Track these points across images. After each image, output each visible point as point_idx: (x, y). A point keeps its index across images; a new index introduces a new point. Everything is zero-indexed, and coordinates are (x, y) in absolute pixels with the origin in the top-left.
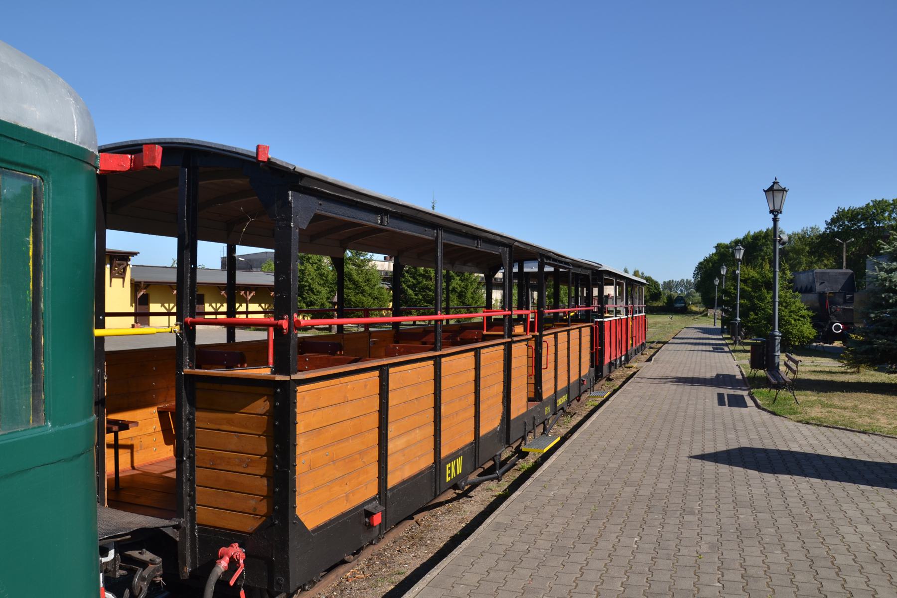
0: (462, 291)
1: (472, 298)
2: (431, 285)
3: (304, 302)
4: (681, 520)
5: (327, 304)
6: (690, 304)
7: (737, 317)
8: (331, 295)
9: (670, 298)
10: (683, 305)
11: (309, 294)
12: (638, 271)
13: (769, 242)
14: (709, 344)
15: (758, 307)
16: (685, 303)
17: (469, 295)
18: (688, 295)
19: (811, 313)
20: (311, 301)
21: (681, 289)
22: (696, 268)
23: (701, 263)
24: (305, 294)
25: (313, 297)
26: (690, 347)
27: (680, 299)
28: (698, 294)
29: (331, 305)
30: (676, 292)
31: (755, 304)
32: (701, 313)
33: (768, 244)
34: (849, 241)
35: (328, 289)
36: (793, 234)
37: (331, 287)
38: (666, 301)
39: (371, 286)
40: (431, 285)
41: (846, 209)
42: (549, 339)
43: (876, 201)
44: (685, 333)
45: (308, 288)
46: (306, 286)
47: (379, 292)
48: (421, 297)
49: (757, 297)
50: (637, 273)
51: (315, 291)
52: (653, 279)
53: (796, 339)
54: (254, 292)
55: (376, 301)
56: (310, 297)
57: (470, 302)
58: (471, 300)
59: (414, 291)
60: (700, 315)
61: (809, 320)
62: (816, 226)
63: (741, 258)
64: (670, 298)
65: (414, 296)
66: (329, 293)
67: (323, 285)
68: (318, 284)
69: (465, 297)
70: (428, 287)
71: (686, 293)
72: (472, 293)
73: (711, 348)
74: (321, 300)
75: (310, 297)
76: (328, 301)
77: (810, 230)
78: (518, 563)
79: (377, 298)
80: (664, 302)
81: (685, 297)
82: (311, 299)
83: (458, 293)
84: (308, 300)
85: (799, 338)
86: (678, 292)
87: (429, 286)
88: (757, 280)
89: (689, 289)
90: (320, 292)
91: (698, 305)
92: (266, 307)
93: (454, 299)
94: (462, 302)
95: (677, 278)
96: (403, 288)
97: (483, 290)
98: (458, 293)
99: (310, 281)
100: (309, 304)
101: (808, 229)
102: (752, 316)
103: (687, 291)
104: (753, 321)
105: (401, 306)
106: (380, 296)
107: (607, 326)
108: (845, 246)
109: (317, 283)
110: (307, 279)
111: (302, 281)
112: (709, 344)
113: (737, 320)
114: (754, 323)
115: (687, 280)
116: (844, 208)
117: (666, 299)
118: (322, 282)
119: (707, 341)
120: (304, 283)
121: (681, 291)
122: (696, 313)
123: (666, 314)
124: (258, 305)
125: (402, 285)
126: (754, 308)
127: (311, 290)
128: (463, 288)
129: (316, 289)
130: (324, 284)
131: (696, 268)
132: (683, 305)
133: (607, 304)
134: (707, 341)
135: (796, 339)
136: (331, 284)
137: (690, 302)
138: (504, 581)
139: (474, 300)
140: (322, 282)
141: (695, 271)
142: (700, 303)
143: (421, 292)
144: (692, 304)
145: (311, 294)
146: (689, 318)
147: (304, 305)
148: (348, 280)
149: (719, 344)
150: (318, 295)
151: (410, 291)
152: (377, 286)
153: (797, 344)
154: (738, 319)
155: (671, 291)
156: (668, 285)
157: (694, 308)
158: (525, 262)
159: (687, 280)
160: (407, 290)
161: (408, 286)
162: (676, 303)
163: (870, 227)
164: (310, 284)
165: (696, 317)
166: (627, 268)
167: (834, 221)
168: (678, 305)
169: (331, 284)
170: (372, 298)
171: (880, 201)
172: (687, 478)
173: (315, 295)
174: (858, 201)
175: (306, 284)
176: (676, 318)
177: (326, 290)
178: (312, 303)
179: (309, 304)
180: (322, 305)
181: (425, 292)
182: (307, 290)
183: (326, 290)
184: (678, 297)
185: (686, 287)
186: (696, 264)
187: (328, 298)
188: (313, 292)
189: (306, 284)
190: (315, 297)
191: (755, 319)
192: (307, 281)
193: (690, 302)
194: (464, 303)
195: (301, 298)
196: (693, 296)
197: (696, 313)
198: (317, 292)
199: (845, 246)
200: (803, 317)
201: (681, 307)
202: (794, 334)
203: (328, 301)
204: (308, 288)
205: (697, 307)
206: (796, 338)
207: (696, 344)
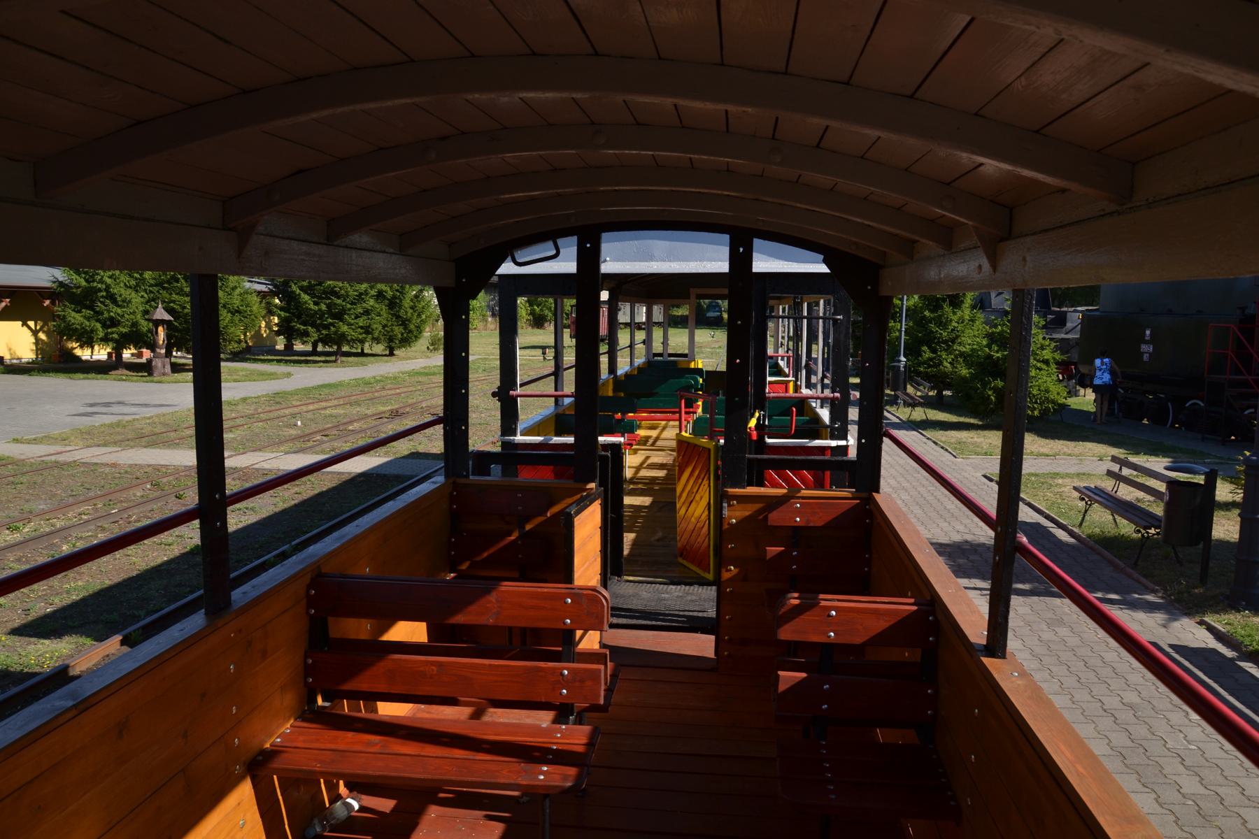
0: (394, 297)
1: (412, 308)
2: (340, 288)
3: (98, 321)
5: (143, 323)
7: (900, 355)
8: (150, 306)
11: (106, 306)
15: (935, 338)
17: (407, 303)
19: (1058, 356)
20: (111, 319)
24: (99, 304)
25: (115, 311)
29: (151, 324)
31: (933, 332)
35: (146, 295)
37: (151, 292)
39: (227, 290)
40: (340, 288)
45: (104, 294)
46: (100, 290)
47: (242, 300)
48: (324, 307)
51: (119, 299)
53: (1036, 406)
54: (8, 300)
55: (237, 318)
56: (109, 311)
57: (409, 314)
58: (411, 311)
59: (312, 295)
61: (1053, 366)
65: (312, 306)
66: (148, 302)
67: (136, 289)
68: (125, 285)
69: (400, 307)
70: (336, 291)
72: (412, 300)
74: (132, 317)
75: (109, 311)
76: (146, 317)
79: (238, 311)
82: (112, 314)
83: (388, 299)
84: (106, 315)
87: (337, 289)
90: (130, 301)
92: (38, 328)
93: (382, 310)
94: (395, 314)
96: (293, 292)
97: (431, 292)
98: (388, 299)
99: (109, 281)
100: (108, 323)
102: (927, 354)
104: (927, 363)
105: (291, 323)
106: (244, 308)
109: (122, 285)
110: (102, 277)
111: (93, 281)
113: (900, 361)
114: (930, 366)
118: (133, 283)
120: (95, 284)
124: (20, 323)
125: (290, 287)
126: (930, 340)
127: (112, 298)
128: (397, 291)
129: (121, 296)
130: (137, 285)
132: (719, 314)
135: (1036, 406)
136: (151, 285)
139: (415, 312)
140: (133, 283)
143: (324, 298)
145: (111, 306)
147: (98, 325)
148: (183, 278)
150: (124, 307)
151: (305, 297)
152: (239, 290)
153: (1036, 413)
154: (903, 359)
158: (605, 236)
160: (299, 295)
161: (301, 288)
164: (108, 287)
168: (710, 314)
169: (151, 285)
170: (229, 311)
173: (118, 306)
175: (99, 286)
177: (142, 297)
178: (113, 323)
179: (108, 323)
180: (135, 324)
181: (330, 299)
182: (102, 297)
183: (142, 297)
187: (146, 312)
188: (114, 301)
189: (99, 286)
190: (119, 311)
191: (931, 359)
192: (101, 281)
194: (398, 317)
195: (92, 313)
198: (123, 301)
200: (1046, 362)
202: (1034, 396)
203: (146, 317)
204: (104, 294)
206: (1036, 403)
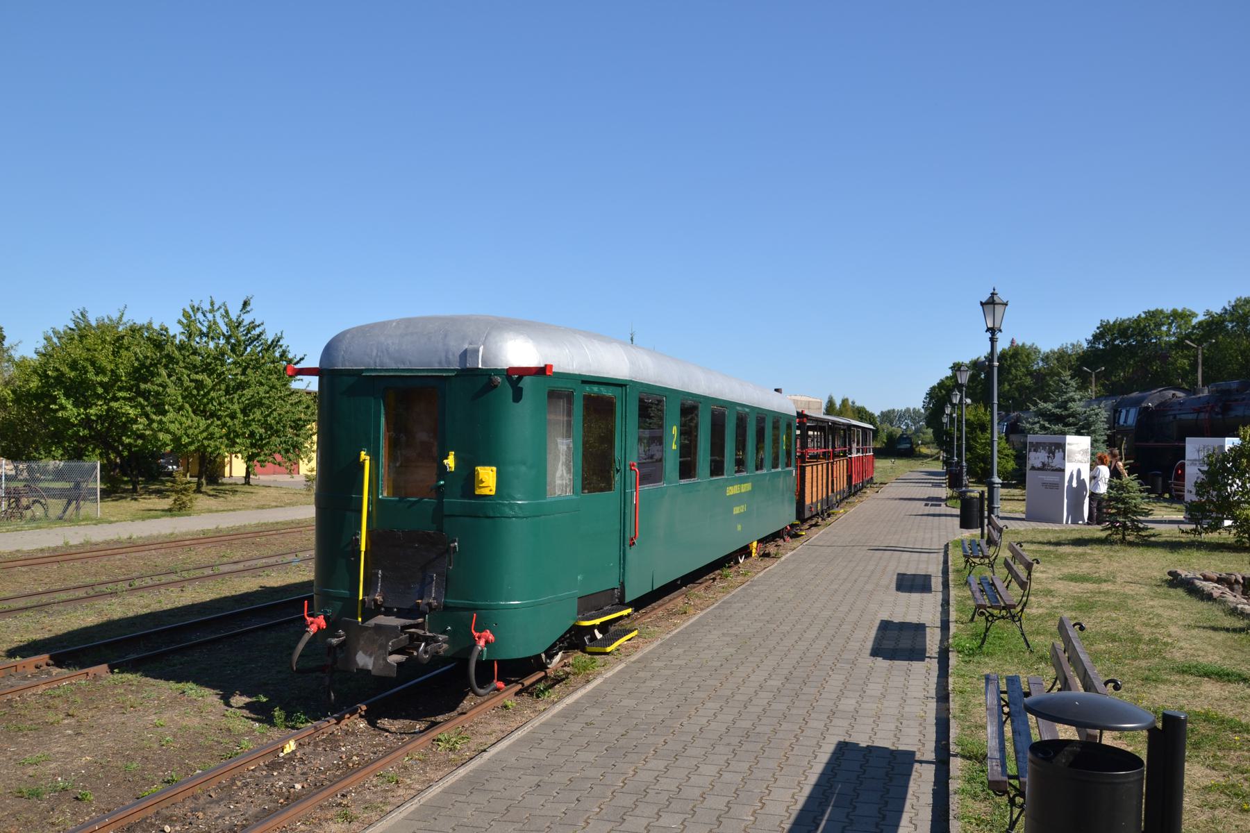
4: (915, 801)
6: (919, 445)
9: (890, 437)
10: (909, 445)
12: (847, 400)
13: (1019, 363)
14: (930, 483)
16: (912, 443)
18: (918, 431)
21: (906, 423)
22: (927, 394)
23: (933, 389)
26: (914, 484)
27: (904, 438)
28: (930, 431)
30: (900, 427)
32: (932, 456)
33: (1018, 365)
34: (1099, 370)
36: (1051, 351)
38: (885, 441)
41: (1111, 323)
42: (808, 470)
43: (1149, 312)
44: (908, 475)
49: (972, 438)
50: (846, 402)
52: (867, 410)
60: (930, 459)
62: (1078, 341)
63: (957, 402)
64: (890, 437)
71: (913, 428)
73: (930, 485)
77: (1071, 347)
78: (699, 802)
80: (884, 442)
81: (913, 434)
85: (1003, 474)
86: (902, 426)
88: (973, 422)
89: (919, 423)
91: (931, 445)
95: (900, 406)
101: (1069, 345)
103: (915, 425)
107: (853, 459)
108: (1093, 376)
112: (930, 483)
115: (914, 409)
116: (1108, 320)
117: (885, 437)
119: (929, 481)
121: (907, 425)
122: (926, 456)
123: (886, 458)
131: (927, 394)
132: (909, 445)
133: (447, 459)
134: (929, 481)
137: (920, 442)
138: (682, 827)
141: (926, 398)
142: (933, 443)
144: (922, 444)
146: (916, 462)
149: (940, 483)
154: (956, 458)
155: (892, 426)
156: (888, 416)
157: (924, 450)
159: (914, 409)
162: (899, 443)
163: (1141, 345)
165: (925, 461)
166: (833, 395)
167: (1097, 338)
171: (1153, 312)
172: (922, 738)
174: (1128, 309)
176: (900, 463)
184: (902, 435)
185: (913, 419)
186: (927, 389)
193: (920, 442)
196: (924, 433)
197: (926, 456)
199: (1093, 376)
200: (1007, 455)
201: (906, 449)
205: (928, 448)
207: (917, 483)
